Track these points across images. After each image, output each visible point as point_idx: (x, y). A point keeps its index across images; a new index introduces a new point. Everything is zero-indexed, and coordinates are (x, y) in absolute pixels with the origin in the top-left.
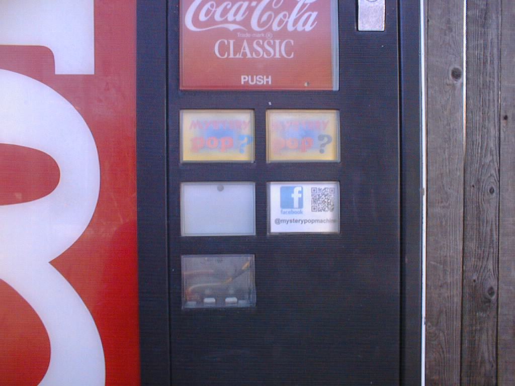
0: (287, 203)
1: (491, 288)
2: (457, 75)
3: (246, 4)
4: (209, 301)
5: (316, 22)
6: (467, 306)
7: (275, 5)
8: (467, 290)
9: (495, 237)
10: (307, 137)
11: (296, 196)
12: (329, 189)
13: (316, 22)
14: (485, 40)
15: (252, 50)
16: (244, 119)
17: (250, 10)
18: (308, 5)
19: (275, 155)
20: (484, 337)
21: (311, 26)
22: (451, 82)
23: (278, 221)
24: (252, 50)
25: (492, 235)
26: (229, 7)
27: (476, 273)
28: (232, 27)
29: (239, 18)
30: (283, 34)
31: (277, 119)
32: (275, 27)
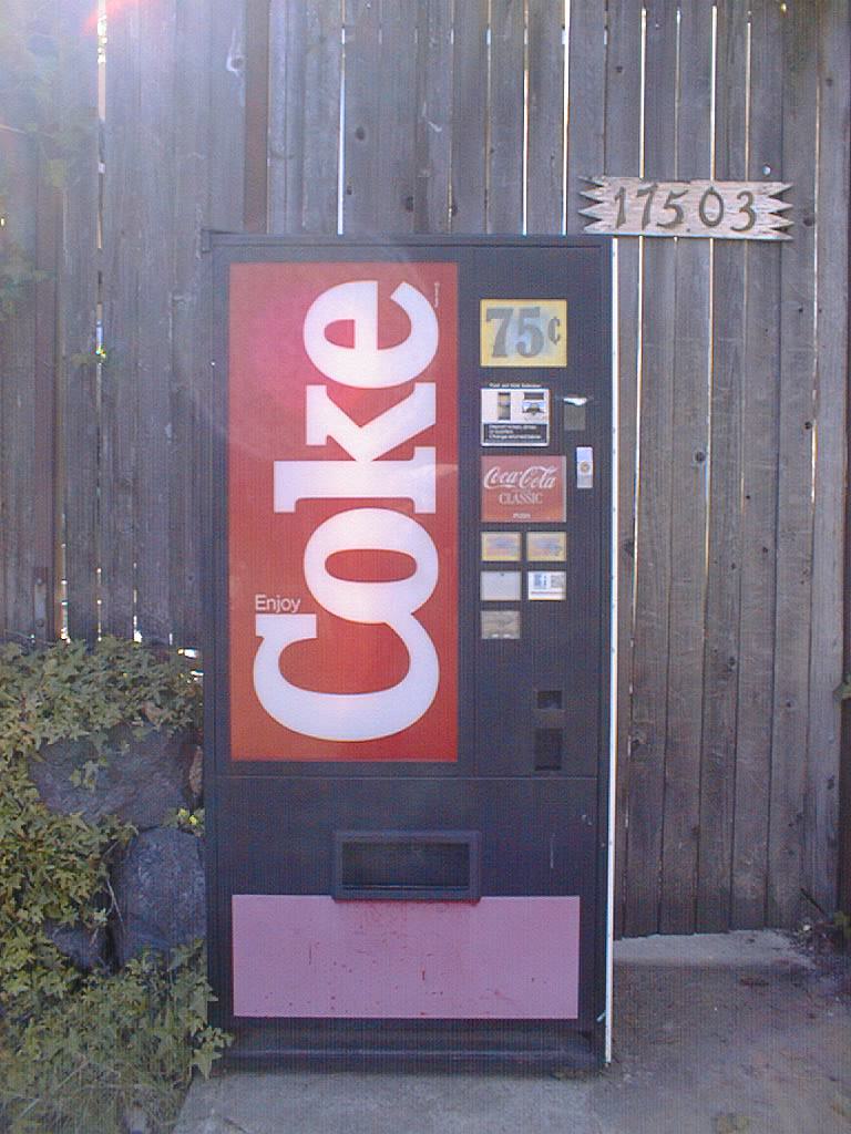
0: (537, 583)
1: (732, 659)
2: (700, 458)
3: (516, 474)
4: (495, 636)
6: (708, 674)
8: (709, 659)
9: (736, 610)
10: (548, 547)
11: (542, 579)
12: (560, 575)
14: (729, 424)
15: (519, 499)
16: (516, 536)
17: (519, 477)
19: (532, 558)
20: (725, 705)
22: (694, 465)
23: (533, 593)
24: (519, 499)
25: (733, 608)
28: (509, 486)
30: (536, 490)
31: (532, 537)
32: (532, 486)
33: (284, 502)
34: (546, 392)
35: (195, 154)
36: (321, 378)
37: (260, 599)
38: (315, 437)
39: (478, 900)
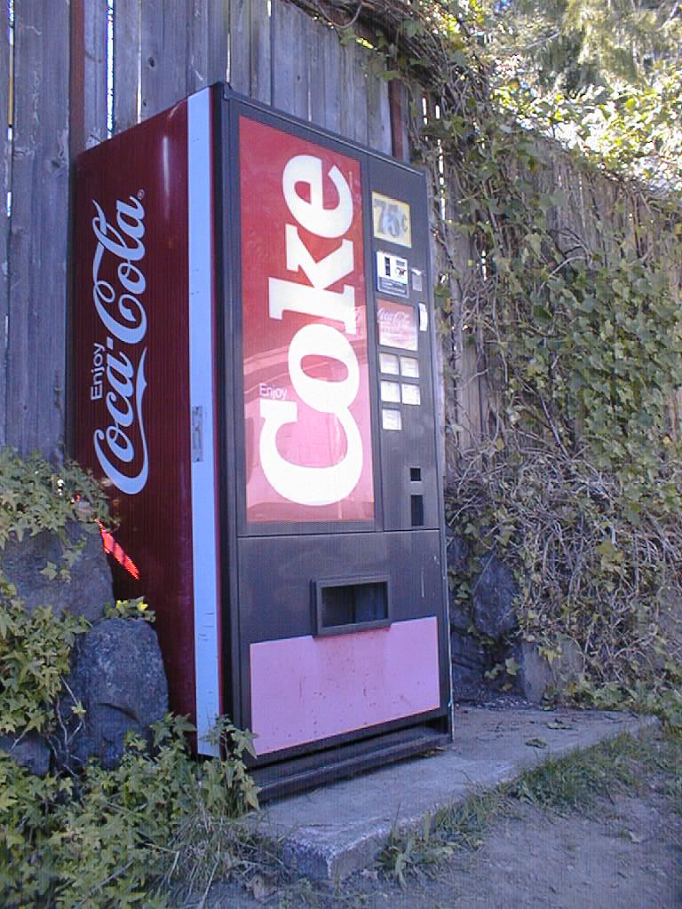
5: (121, 354)
7: (110, 297)
13: (121, 354)
18: (109, 226)
21: (126, 364)
26: (114, 399)
27: (327, 37)
29: (127, 371)
33: (276, 312)
34: (405, 261)
35: (33, 28)
36: (295, 223)
37: (263, 387)
38: (292, 265)
39: (389, 626)
